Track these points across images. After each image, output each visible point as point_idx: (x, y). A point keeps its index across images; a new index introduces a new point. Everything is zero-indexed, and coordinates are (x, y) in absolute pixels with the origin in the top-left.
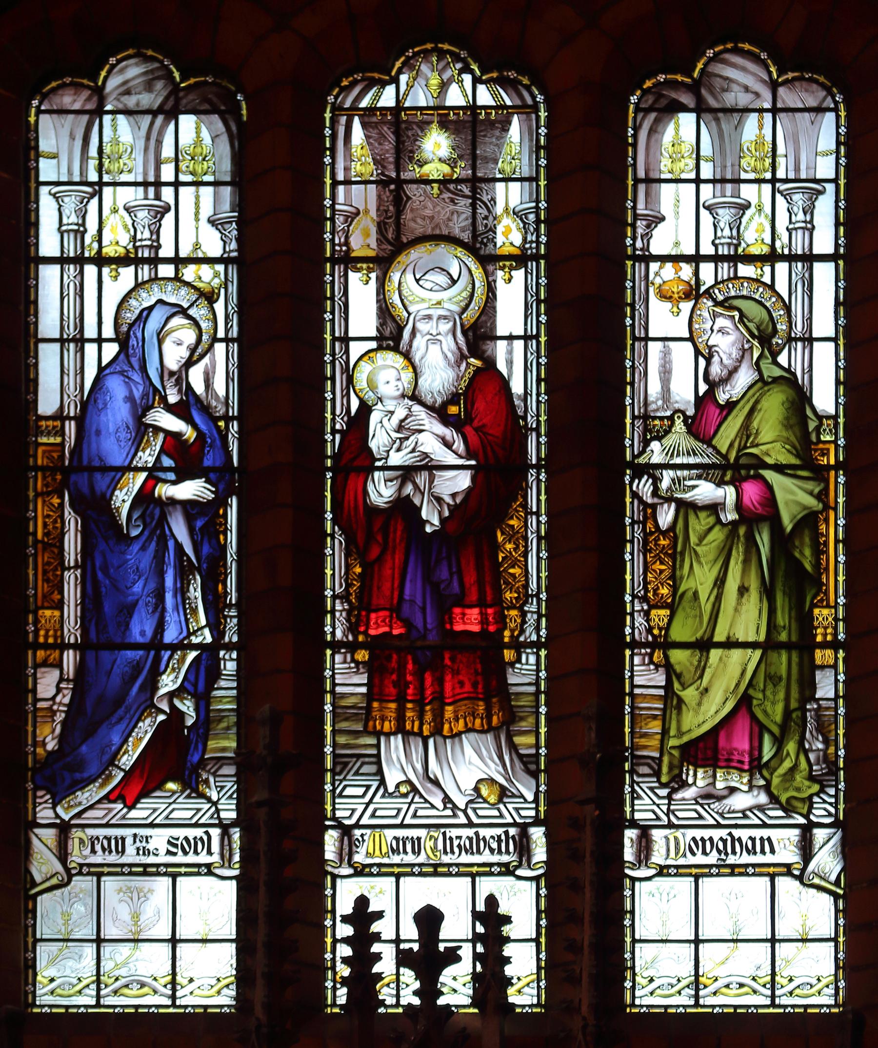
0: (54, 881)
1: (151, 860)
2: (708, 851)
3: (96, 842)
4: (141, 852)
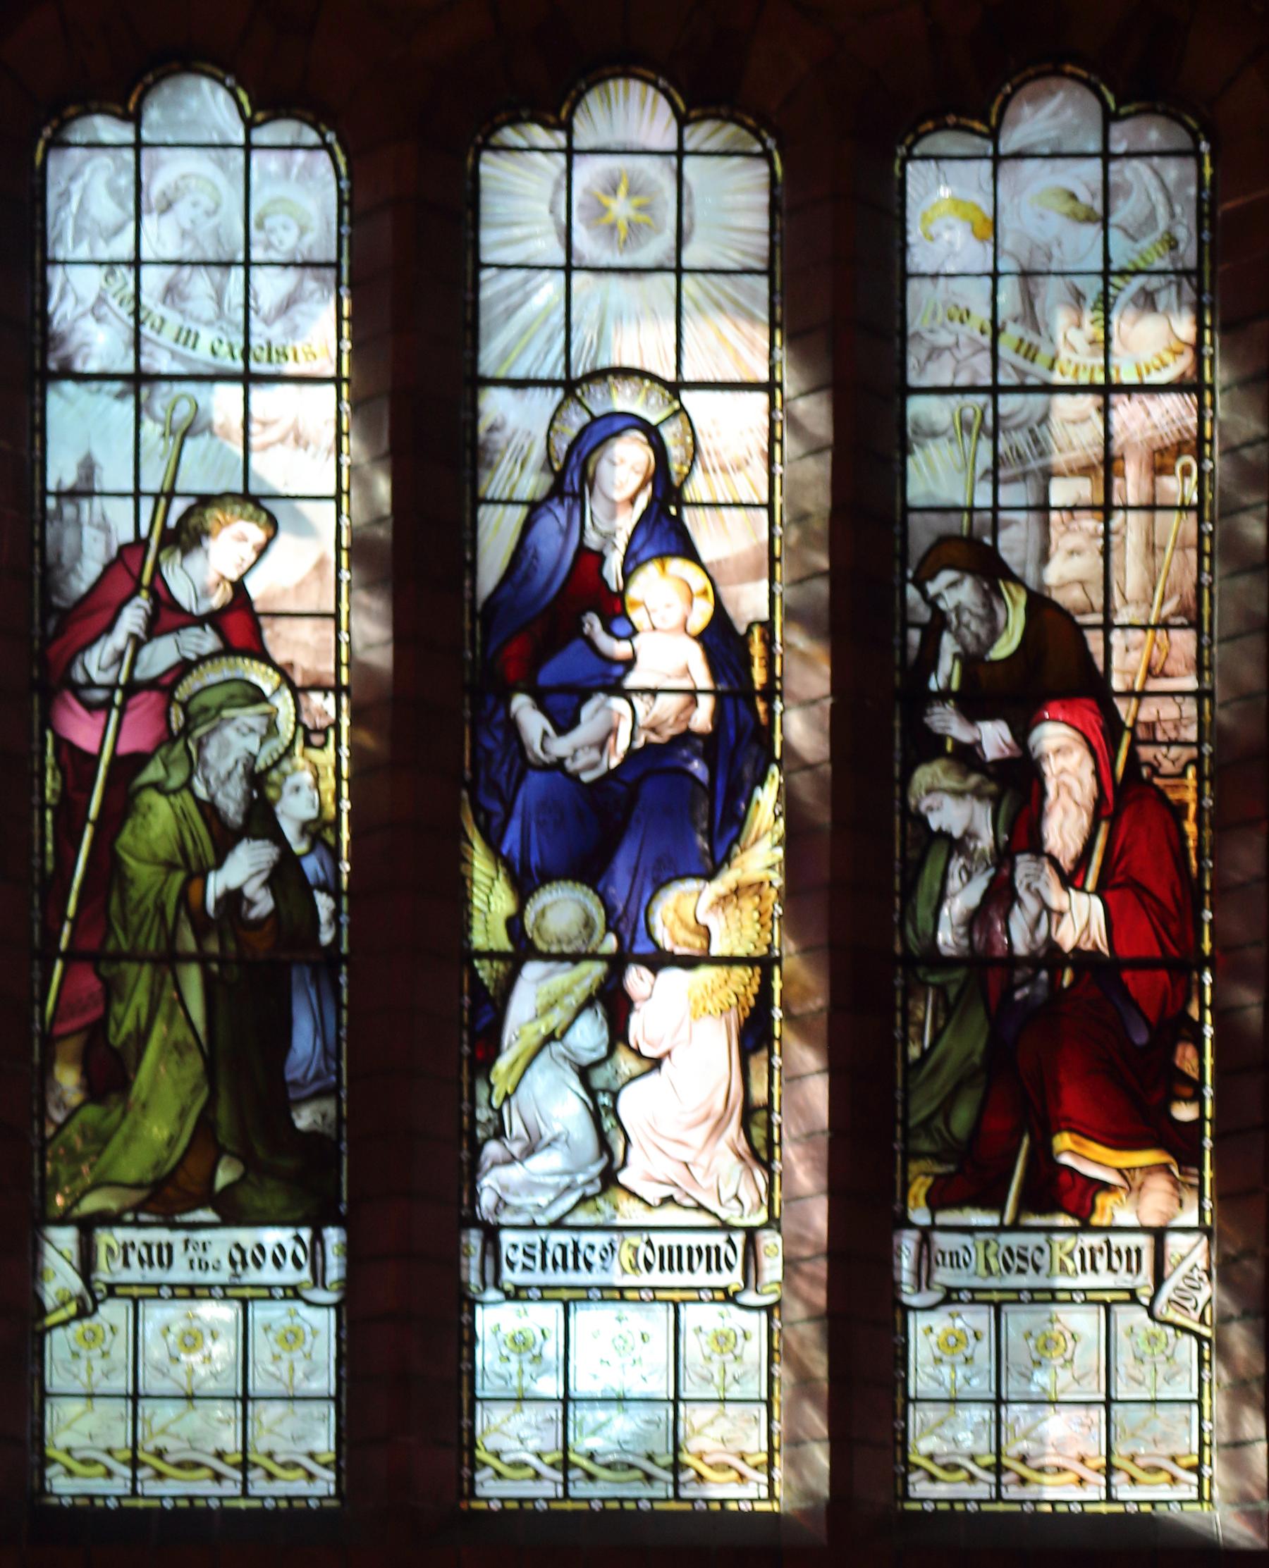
3: (130, 1250)
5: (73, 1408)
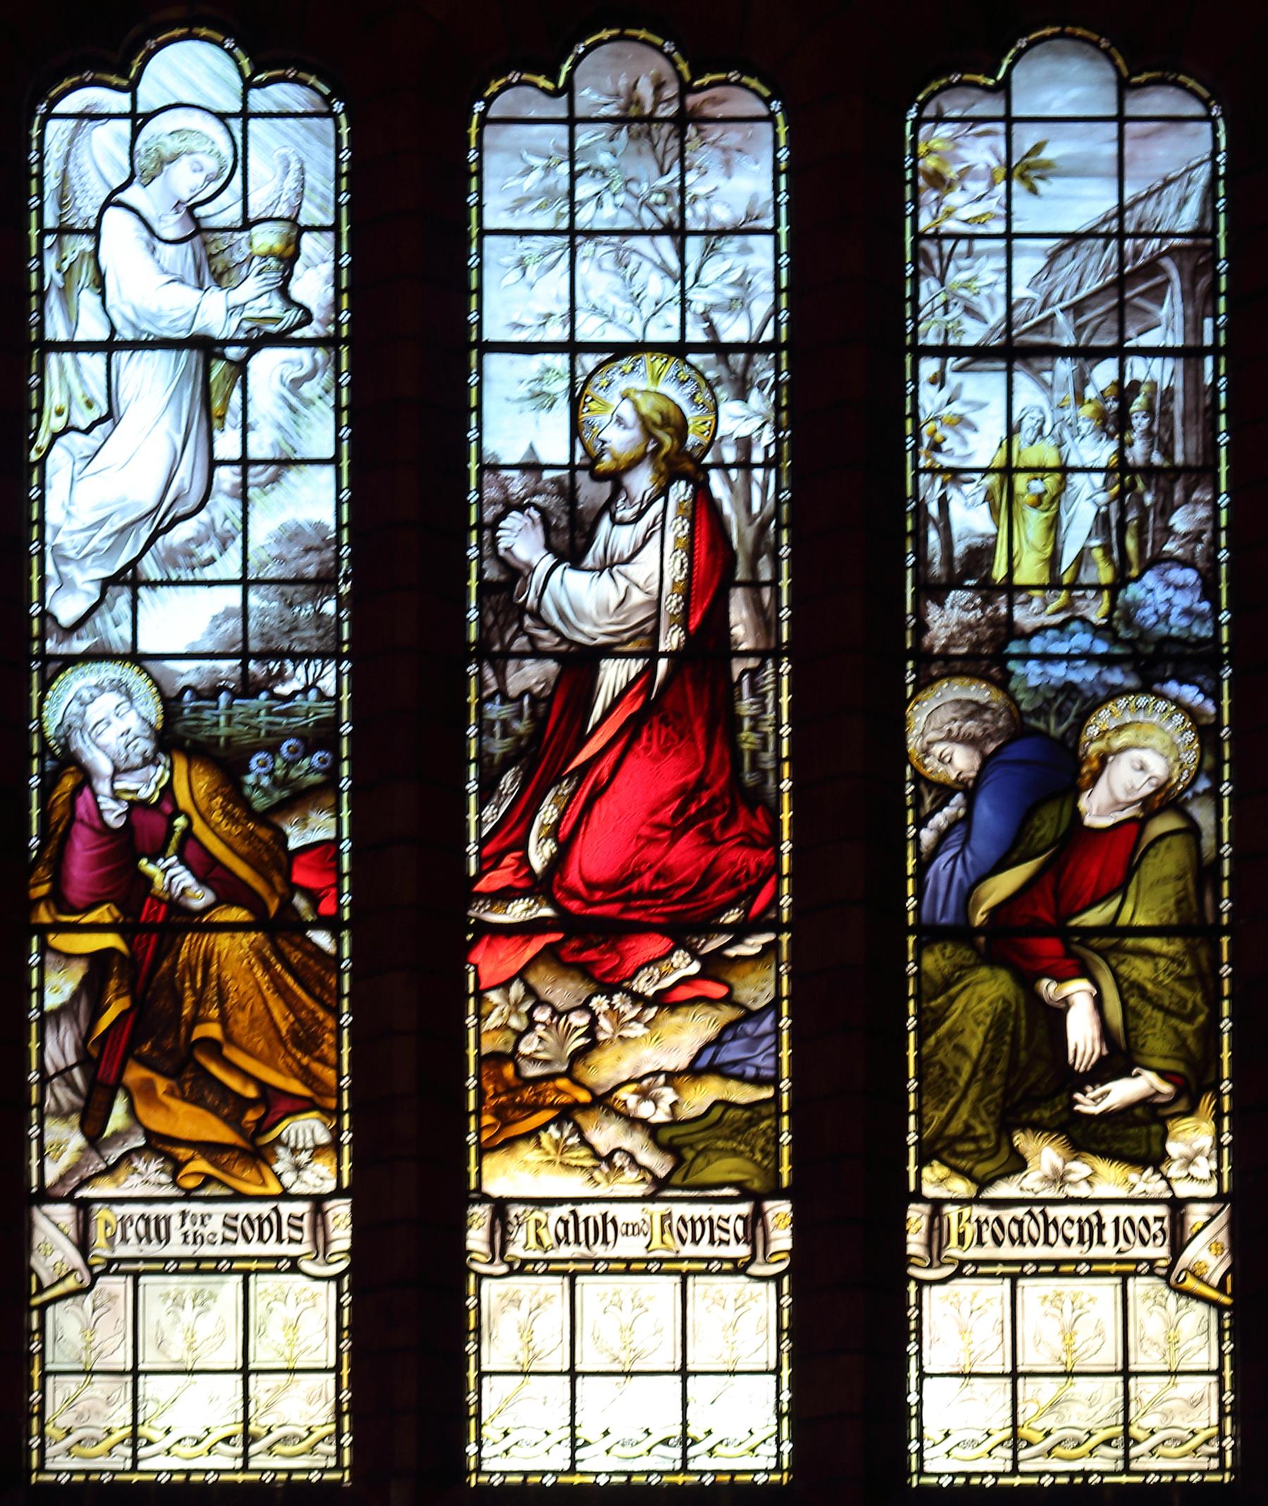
0: (70, 1283)
1: (207, 1251)
2: (266, 1235)
4: (190, 1239)
5: (70, 1385)
